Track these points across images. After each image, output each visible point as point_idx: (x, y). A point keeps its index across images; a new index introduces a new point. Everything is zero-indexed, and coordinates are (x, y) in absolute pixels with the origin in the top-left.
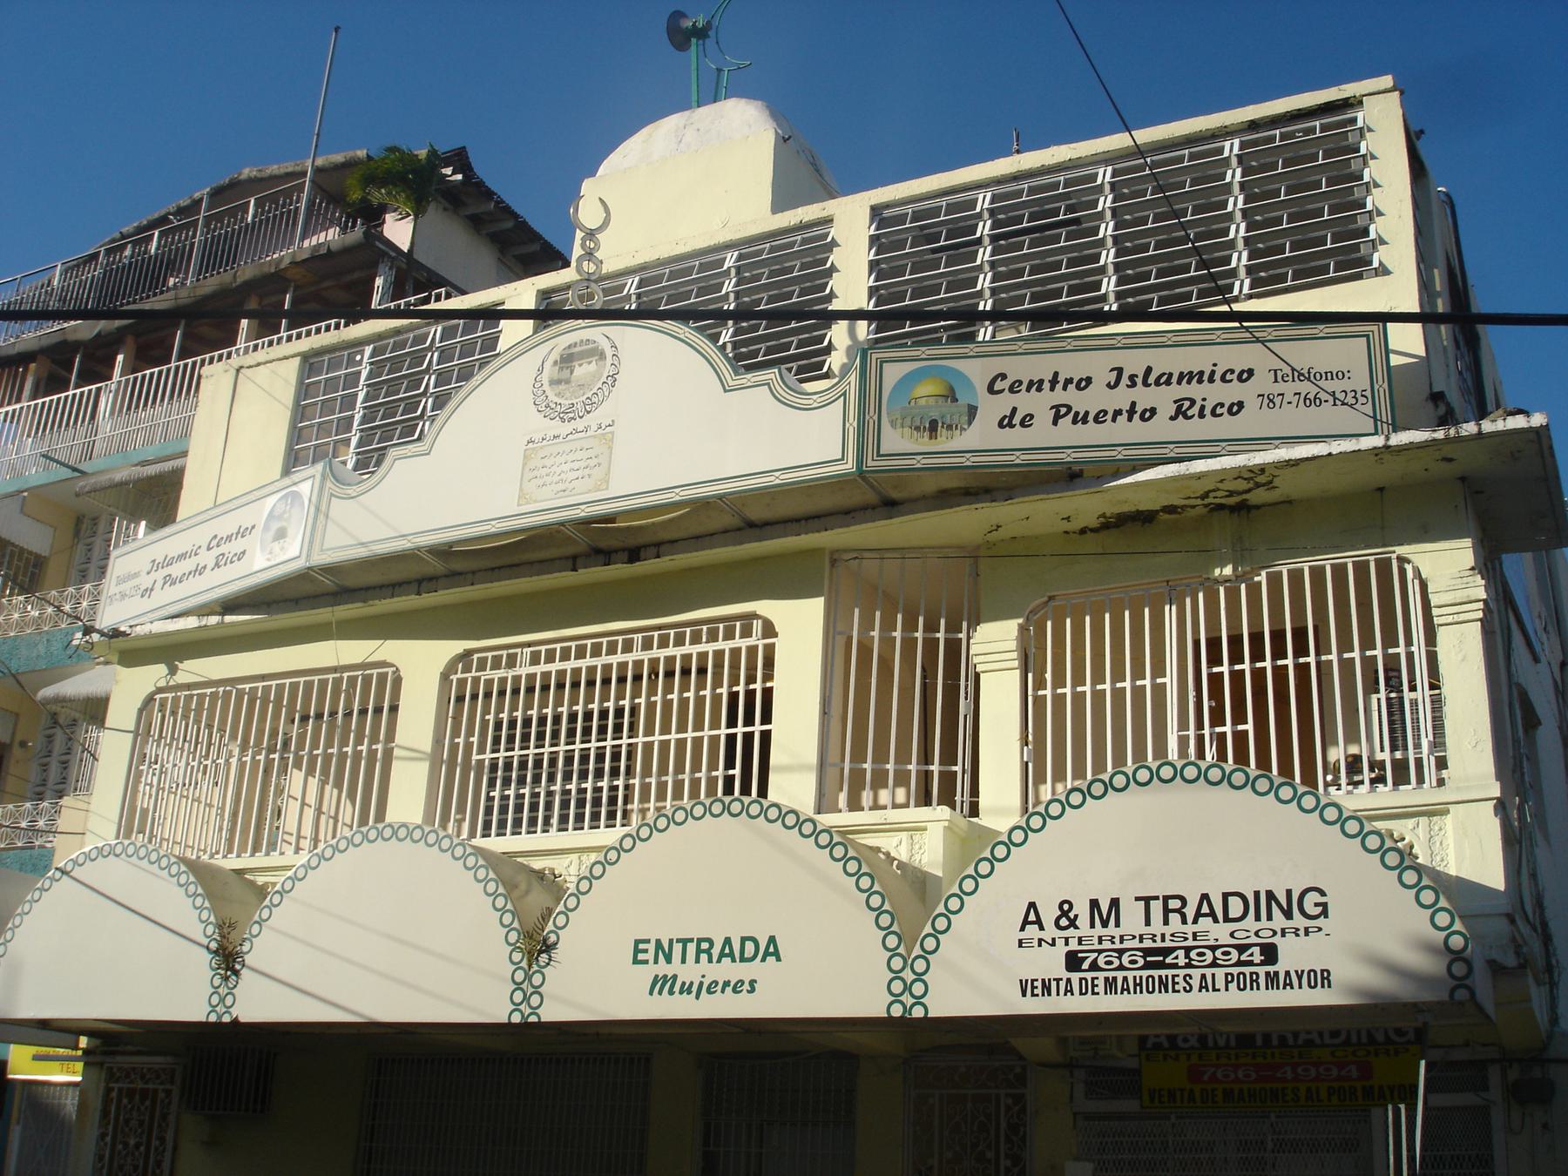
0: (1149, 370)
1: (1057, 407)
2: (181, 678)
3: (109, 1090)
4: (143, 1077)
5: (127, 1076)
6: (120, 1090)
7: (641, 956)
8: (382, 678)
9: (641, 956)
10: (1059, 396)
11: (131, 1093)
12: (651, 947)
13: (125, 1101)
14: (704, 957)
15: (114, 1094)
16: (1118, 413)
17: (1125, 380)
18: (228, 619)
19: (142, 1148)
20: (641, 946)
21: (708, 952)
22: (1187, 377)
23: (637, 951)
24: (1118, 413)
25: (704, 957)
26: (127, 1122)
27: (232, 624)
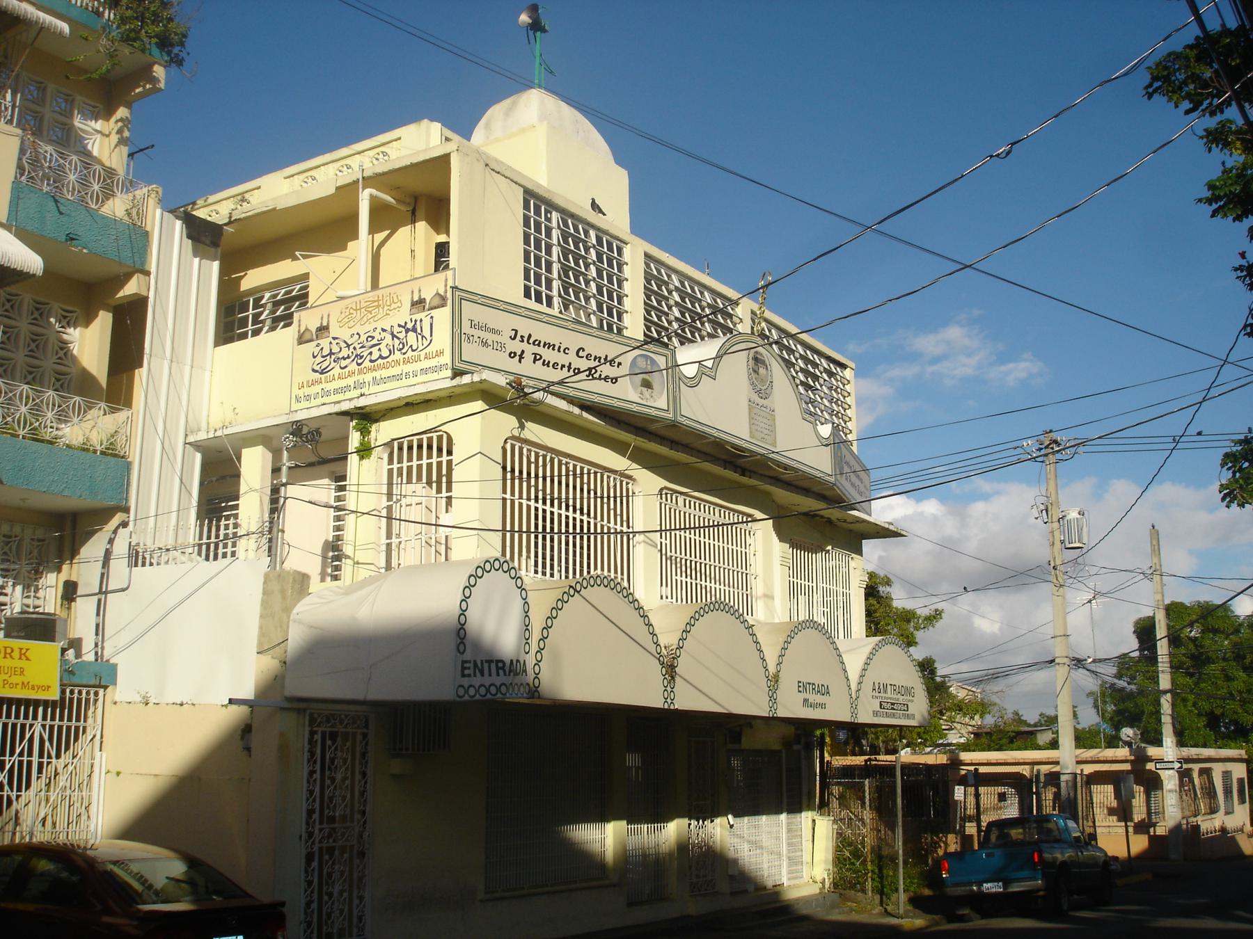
0: (530, 336)
1: (535, 354)
2: (526, 434)
3: (312, 733)
4: (341, 722)
5: (328, 721)
6: (324, 734)
7: (466, 672)
8: (440, 438)
9: (466, 672)
10: (540, 350)
11: (333, 736)
12: (471, 665)
13: (329, 742)
14: (501, 672)
15: (318, 737)
16: (563, 366)
17: (518, 338)
18: (585, 415)
19: (348, 782)
20: (467, 665)
21: (503, 668)
22: (548, 345)
23: (464, 668)
24: (563, 366)
25: (501, 672)
26: (332, 760)
27: (586, 420)
